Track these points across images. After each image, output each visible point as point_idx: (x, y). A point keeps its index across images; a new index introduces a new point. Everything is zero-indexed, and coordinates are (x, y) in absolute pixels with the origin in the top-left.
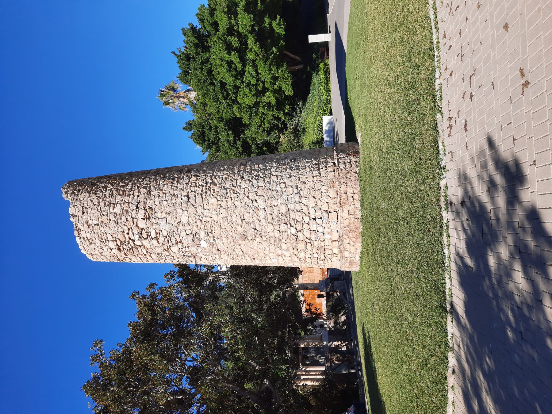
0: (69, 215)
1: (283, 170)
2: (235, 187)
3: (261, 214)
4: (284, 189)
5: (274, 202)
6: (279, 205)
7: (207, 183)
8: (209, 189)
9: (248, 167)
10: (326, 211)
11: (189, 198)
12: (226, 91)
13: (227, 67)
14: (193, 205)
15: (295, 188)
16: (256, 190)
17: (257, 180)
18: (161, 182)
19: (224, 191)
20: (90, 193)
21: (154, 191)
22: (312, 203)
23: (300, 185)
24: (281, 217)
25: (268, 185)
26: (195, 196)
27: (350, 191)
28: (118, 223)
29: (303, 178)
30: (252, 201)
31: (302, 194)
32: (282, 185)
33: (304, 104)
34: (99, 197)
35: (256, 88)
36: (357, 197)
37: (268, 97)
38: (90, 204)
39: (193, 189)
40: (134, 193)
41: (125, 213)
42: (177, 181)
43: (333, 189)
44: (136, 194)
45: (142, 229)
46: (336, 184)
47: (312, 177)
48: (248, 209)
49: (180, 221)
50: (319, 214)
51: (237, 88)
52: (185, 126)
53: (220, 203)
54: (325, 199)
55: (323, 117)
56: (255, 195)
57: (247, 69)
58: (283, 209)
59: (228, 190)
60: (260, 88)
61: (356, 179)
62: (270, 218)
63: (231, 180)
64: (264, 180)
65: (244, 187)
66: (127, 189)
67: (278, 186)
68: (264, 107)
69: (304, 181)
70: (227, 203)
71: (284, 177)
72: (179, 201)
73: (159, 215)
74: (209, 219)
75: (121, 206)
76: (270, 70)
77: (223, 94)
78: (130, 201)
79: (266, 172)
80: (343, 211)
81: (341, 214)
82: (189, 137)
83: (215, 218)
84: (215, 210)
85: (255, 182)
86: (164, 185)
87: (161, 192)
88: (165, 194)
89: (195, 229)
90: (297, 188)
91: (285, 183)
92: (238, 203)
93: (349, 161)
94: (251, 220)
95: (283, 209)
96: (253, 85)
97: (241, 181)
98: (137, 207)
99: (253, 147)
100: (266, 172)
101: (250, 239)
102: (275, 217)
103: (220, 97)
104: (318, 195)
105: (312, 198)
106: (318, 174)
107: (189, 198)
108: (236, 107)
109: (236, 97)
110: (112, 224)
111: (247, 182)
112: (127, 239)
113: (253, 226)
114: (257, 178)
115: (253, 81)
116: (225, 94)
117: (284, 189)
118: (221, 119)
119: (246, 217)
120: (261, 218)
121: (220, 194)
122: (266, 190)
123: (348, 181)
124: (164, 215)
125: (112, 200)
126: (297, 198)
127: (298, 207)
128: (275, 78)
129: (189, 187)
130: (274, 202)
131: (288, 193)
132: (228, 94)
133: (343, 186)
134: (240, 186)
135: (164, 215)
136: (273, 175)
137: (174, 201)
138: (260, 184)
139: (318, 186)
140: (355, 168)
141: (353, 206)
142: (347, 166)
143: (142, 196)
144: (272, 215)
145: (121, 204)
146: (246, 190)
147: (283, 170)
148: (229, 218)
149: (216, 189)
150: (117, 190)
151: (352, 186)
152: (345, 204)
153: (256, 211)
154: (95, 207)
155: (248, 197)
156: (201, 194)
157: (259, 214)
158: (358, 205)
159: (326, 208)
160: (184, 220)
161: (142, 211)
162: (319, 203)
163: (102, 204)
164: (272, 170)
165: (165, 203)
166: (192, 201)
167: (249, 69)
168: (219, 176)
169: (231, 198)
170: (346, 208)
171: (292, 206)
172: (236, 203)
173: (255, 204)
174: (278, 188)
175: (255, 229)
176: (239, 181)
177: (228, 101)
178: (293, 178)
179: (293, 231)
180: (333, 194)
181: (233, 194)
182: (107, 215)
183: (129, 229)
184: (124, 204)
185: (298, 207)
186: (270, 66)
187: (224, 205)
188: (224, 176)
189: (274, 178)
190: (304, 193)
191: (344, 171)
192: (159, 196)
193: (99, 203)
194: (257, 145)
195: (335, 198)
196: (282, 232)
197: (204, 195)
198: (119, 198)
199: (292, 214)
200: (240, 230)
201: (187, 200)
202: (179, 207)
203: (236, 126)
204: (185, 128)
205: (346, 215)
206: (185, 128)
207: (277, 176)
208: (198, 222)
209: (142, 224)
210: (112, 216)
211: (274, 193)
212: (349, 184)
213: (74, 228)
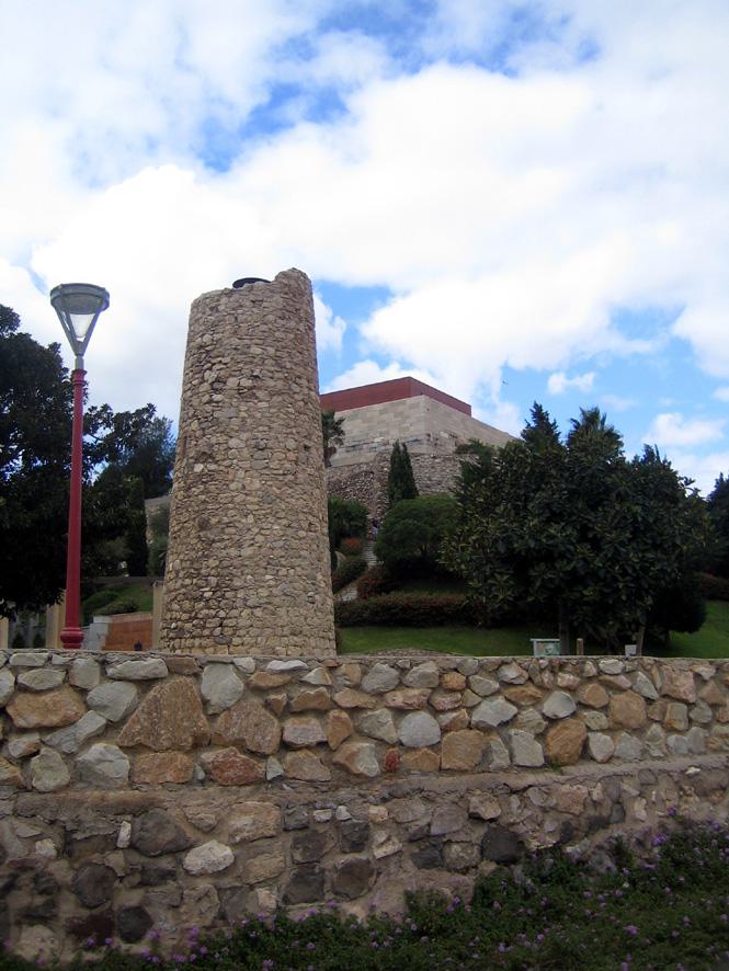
3: (233, 552)
28: (235, 349)
44: (277, 375)
58: (237, 583)
62: (225, 563)
73: (243, 408)
84: (244, 487)
85: (281, 543)
94: (226, 537)
101: (201, 534)
104: (254, 631)
105: (249, 622)
143: (272, 383)
160: (233, 442)
161: (249, 383)
162: (242, 632)
163: (264, 328)
166: (258, 454)
175: (214, 541)
179: (208, 595)
183: (225, 364)
185: (239, 603)
190: (258, 612)
200: (214, 521)
209: (232, 382)
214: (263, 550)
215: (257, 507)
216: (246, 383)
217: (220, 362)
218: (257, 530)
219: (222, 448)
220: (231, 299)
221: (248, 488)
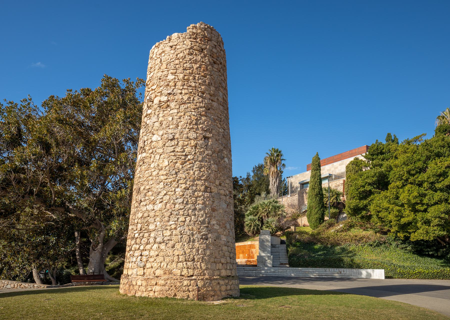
0: (170, 34)
1: (190, 227)
2: (178, 182)
3: (150, 207)
4: (169, 228)
5: (158, 219)
6: (155, 223)
7: (186, 155)
8: (178, 158)
9: (200, 194)
10: (145, 265)
11: (171, 140)
12: (417, 172)
13: (439, 173)
14: (165, 145)
15: (168, 238)
16: (172, 201)
17: (183, 202)
18: (193, 113)
19: (174, 172)
20: (189, 49)
21: (184, 108)
22: (153, 253)
23: (171, 243)
24: (146, 224)
25: (175, 213)
26: (173, 146)
27: (157, 288)
29: (178, 246)
30: (162, 198)
31: (163, 244)
32: (173, 227)
33: (410, 251)
34: (185, 57)
35: (417, 204)
36: (151, 294)
37: (408, 216)
38: (179, 51)
39: (181, 143)
40: (185, 89)
41: (166, 84)
42: (192, 128)
43: (162, 273)
45: (153, 102)
46: (166, 277)
47: (177, 254)
48: (155, 195)
49: (154, 134)
50: (144, 259)
51: (420, 185)
52: (392, 135)
53: (163, 169)
54: (155, 265)
55: (383, 270)
56: (166, 201)
57: (439, 193)
59: (175, 176)
60: (418, 207)
61: (168, 295)
63: (185, 179)
64: (181, 209)
65: (177, 190)
66: (191, 82)
67: (174, 222)
68: (398, 211)
69: (176, 246)
70: (162, 175)
71: (182, 228)
72: (170, 131)
74: (152, 160)
75: (173, 79)
76: (436, 218)
77: (413, 170)
78: (177, 87)
79: (190, 211)
80: (142, 280)
81: (140, 279)
82: (377, 141)
83: (152, 166)
84: (158, 165)
85: (180, 200)
86: (190, 116)
87: (182, 114)
88: (180, 118)
89: (147, 148)
90: (169, 240)
91: (175, 229)
92: (161, 185)
93: (191, 290)
95: (152, 227)
96: (421, 201)
97: (183, 187)
98: (170, 94)
99: (365, 202)
100: (190, 211)
102: (146, 220)
103: (409, 167)
104: (160, 259)
106: (180, 260)
107: (171, 140)
108: (399, 183)
109: (411, 183)
110: (160, 74)
111: (181, 193)
112: (149, 90)
113: (143, 199)
114: (185, 202)
115: (425, 201)
116: (413, 172)
117: (169, 228)
118: (390, 169)
119: (150, 193)
120: (147, 206)
121: (171, 169)
122: (170, 210)
123: (167, 288)
124: (161, 119)
125: (180, 70)
126: (158, 240)
127: (152, 240)
128: (427, 222)
129: (184, 139)
130: (158, 219)
131: (164, 232)
132: (413, 175)
133: (163, 282)
134: (178, 187)
135: (161, 119)
136: (185, 218)
137: (171, 127)
138: (177, 206)
139: (167, 259)
140: (180, 295)
141: (144, 290)
142: (184, 288)
144: (148, 216)
145: (175, 79)
146: (173, 193)
147: (190, 227)
148: (150, 178)
149: (178, 165)
150: (191, 74)
151: (162, 291)
152: (147, 282)
153: (153, 202)
154: (175, 56)
155: (165, 195)
156: (174, 151)
157: (150, 205)
158: (145, 294)
159: (148, 265)
160: (155, 138)
162: (151, 260)
163: (177, 62)
164: (193, 217)
165: (170, 119)
167: (438, 195)
168: (193, 166)
169: (166, 179)
170: (144, 283)
171: (152, 235)
172: (162, 183)
173: (158, 202)
174: (171, 223)
176: (184, 186)
177: (406, 175)
178: (180, 237)
179: (136, 235)
180: (158, 272)
181: (170, 180)
182: (166, 68)
184: (174, 81)
185: (152, 240)
186: (439, 217)
187: (161, 173)
188: (192, 172)
189: (182, 219)
190: (163, 246)
191: (178, 284)
192: (178, 113)
193: (178, 59)
194: (366, 206)
195: (155, 274)
196: (137, 226)
197: (173, 154)
198: (181, 76)
199: (146, 235)
200: (142, 188)
201: (170, 138)
202: (165, 132)
203: (382, 183)
204: (389, 135)
205: (139, 283)
206: (389, 135)
207: (184, 222)
208: (151, 151)
209: (156, 101)
210: (165, 73)
211: (167, 219)
212: (164, 288)
213: (161, 42)
214: (168, 205)
215: (165, 177)
216: (164, 98)
217: (152, 90)
218: (165, 192)
219: (149, 143)
220: (160, 48)
221: (161, 165)
